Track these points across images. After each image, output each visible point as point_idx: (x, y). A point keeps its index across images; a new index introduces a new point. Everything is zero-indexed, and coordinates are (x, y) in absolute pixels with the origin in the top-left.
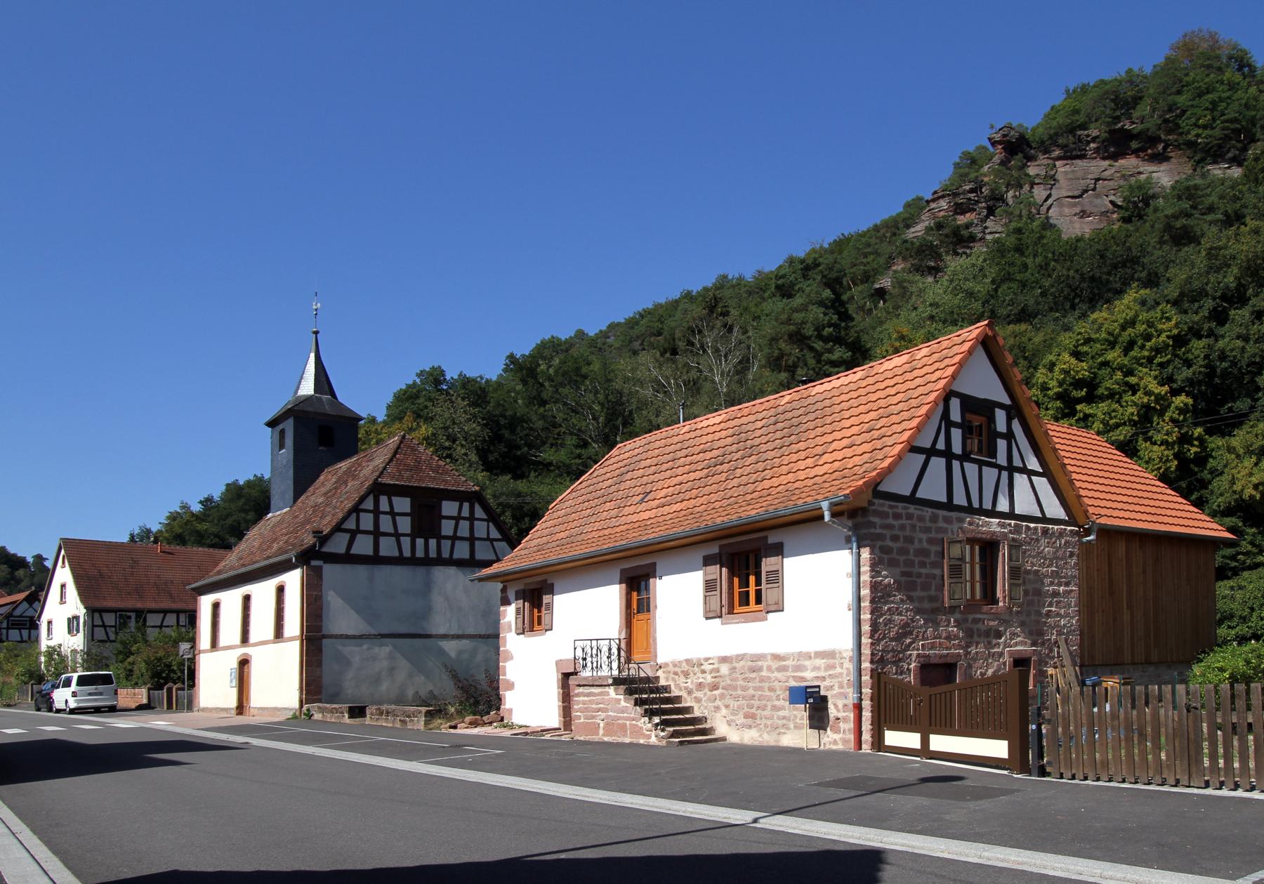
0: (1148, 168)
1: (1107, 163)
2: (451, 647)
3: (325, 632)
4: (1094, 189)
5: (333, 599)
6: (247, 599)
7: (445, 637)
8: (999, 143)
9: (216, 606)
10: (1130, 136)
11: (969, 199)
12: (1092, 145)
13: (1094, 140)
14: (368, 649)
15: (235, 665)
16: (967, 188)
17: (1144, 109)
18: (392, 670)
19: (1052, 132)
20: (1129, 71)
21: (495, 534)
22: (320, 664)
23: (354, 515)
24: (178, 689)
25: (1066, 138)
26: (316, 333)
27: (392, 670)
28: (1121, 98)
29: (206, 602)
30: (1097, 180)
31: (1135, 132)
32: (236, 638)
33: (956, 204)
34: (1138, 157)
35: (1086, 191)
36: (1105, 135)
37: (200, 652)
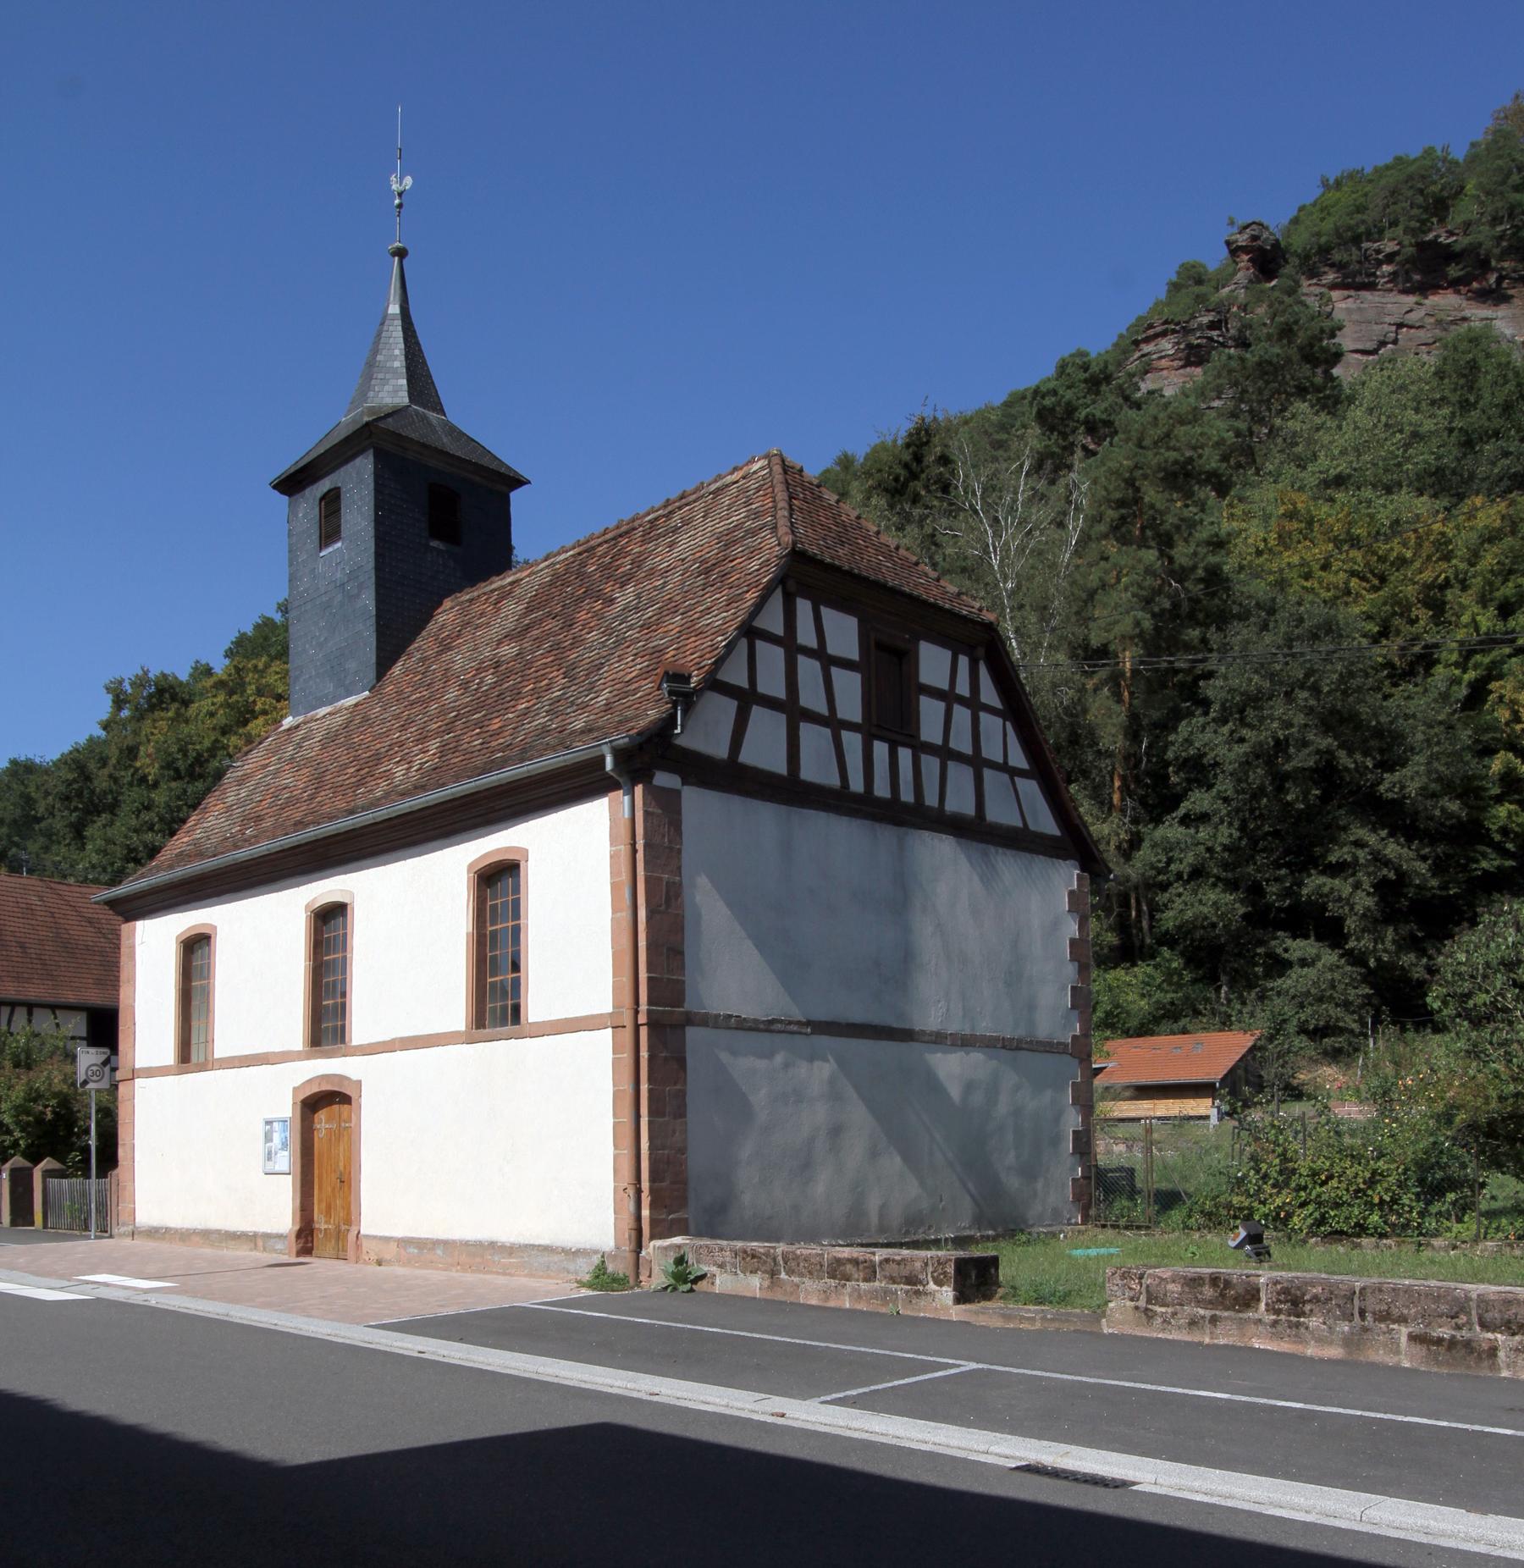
0: (1478, 313)
1: (1411, 299)
2: (950, 1067)
3: (689, 1006)
4: (1395, 342)
5: (707, 905)
6: (329, 922)
7: (939, 1039)
8: (1244, 249)
9: (195, 947)
10: (1448, 255)
11: (1211, 339)
12: (1386, 268)
13: (1390, 258)
14: (786, 1066)
15: (285, 1108)
16: (1205, 320)
17: (1465, 210)
18: (836, 1131)
19: (1323, 240)
20: (1429, 152)
21: (1018, 759)
22: (680, 1112)
23: (744, 643)
24: (48, 1174)
25: (1344, 254)
26: (401, 253)
27: (836, 1131)
28: (1427, 191)
29: (153, 944)
30: (1400, 326)
31: (1457, 248)
32: (292, 1028)
33: (1190, 346)
34: (1458, 292)
35: (1383, 344)
36: (1410, 250)
37: (134, 1074)
